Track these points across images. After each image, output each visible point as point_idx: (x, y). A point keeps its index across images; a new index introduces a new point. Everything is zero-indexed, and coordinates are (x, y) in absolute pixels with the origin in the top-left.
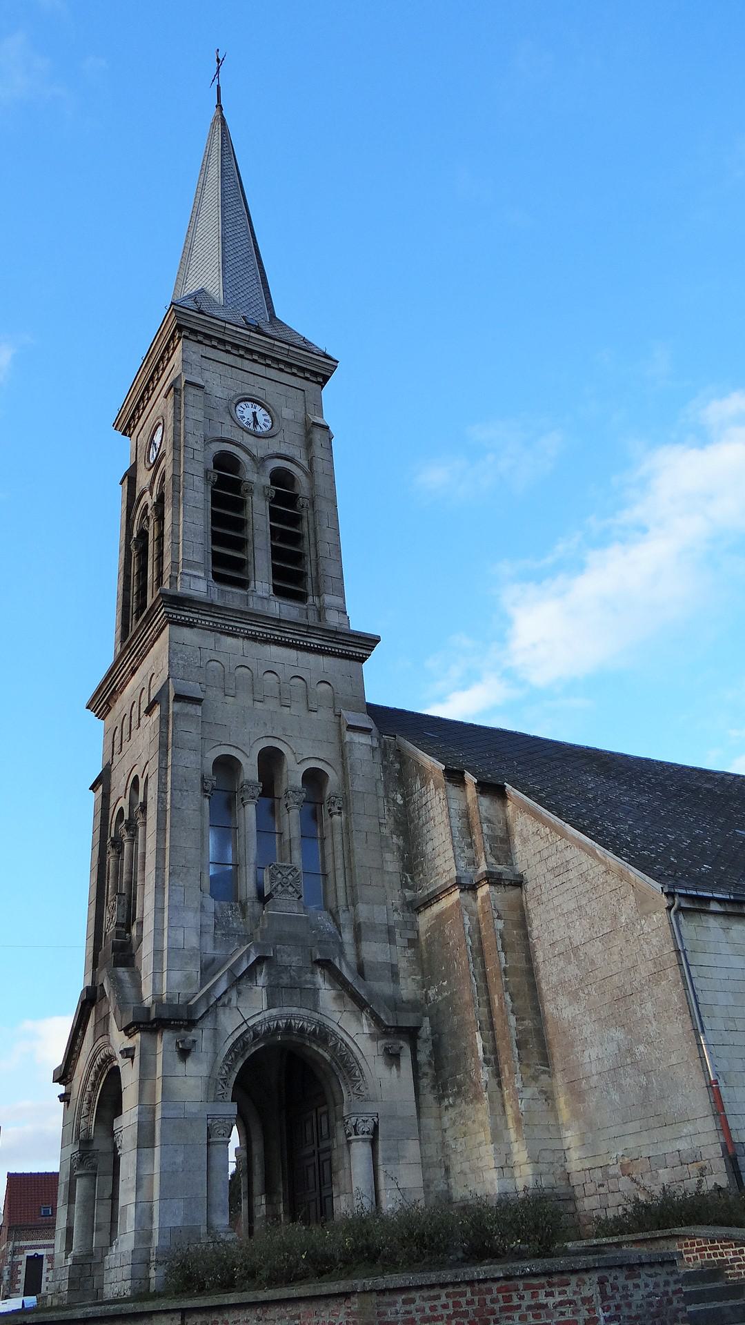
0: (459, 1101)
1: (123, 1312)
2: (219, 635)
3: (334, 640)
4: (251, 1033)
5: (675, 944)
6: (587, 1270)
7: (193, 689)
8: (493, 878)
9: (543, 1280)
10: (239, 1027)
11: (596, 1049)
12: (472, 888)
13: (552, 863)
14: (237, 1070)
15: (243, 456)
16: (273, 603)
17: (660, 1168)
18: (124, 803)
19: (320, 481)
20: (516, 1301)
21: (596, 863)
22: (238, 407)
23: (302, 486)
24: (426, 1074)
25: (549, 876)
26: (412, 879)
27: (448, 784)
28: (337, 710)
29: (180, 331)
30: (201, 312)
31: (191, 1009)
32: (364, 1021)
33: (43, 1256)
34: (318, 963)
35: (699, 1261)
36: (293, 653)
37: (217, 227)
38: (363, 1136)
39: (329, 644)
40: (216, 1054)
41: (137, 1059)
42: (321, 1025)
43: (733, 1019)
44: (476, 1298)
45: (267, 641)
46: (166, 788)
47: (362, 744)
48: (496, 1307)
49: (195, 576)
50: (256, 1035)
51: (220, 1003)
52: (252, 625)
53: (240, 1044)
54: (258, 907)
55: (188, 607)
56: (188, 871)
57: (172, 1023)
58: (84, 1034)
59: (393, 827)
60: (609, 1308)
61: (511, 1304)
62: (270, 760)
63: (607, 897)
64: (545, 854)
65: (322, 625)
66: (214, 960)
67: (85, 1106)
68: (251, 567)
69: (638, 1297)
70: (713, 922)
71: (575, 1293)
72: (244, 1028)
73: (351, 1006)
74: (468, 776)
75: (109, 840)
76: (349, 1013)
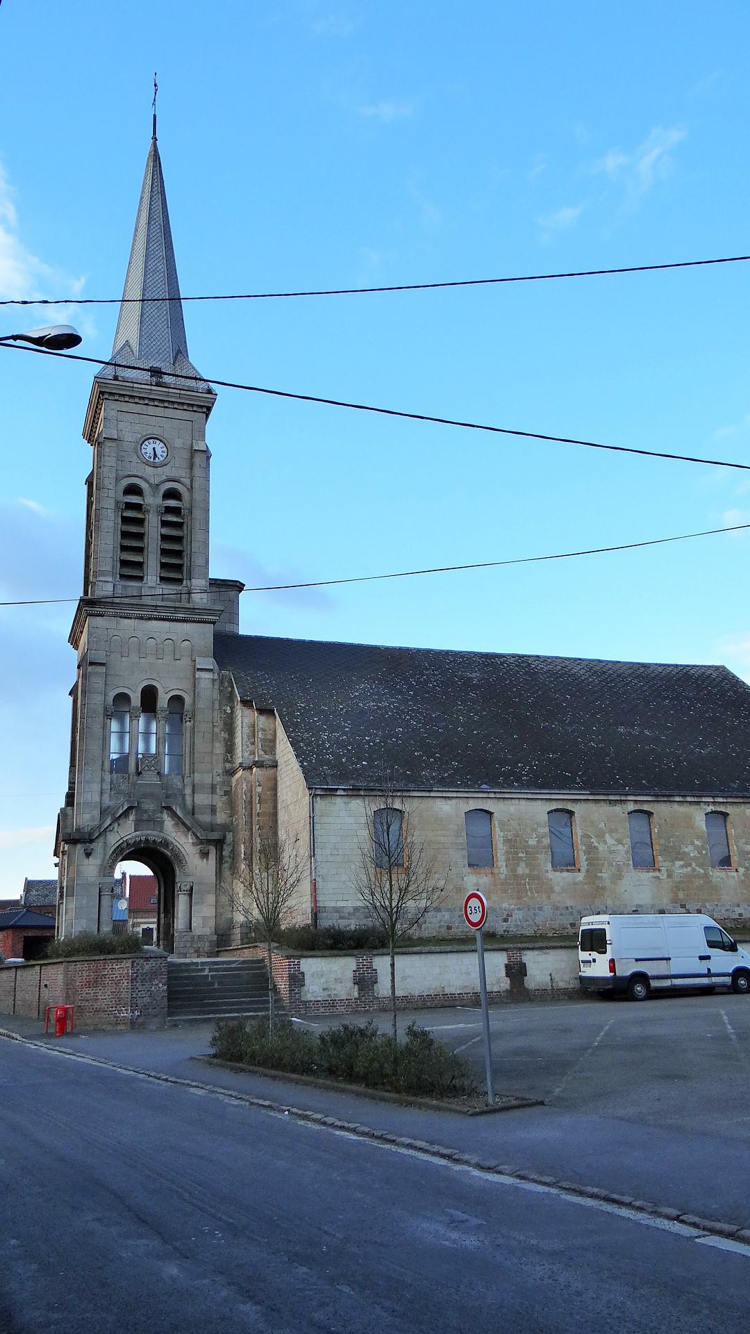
2: (119, 619)
5: (310, 814)
6: (129, 959)
7: (100, 656)
9: (116, 961)
12: (250, 768)
15: (144, 485)
19: (197, 496)
20: (107, 967)
22: (143, 446)
24: (226, 862)
26: (231, 757)
28: (193, 658)
29: (103, 395)
31: (90, 834)
32: (190, 836)
33: (153, 929)
34: (163, 807)
36: (167, 624)
38: (185, 892)
39: (191, 616)
40: (105, 854)
42: (166, 840)
43: (337, 850)
45: (150, 619)
47: (206, 679)
49: (105, 582)
50: (128, 845)
54: (135, 778)
62: (149, 696)
65: (190, 606)
68: (145, 566)
69: (147, 967)
70: (338, 800)
72: (121, 841)
73: (183, 829)
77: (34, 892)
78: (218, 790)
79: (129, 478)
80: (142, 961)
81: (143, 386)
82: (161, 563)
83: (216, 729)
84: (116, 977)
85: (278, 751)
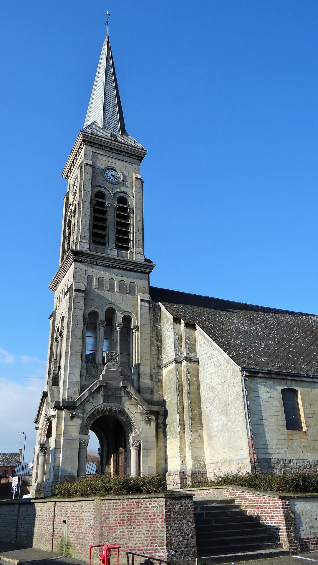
0: (171, 437)
1: (22, 502)
2: (93, 265)
3: (137, 266)
4: (97, 411)
5: (243, 389)
8: (188, 359)
9: (149, 500)
10: (92, 409)
13: (208, 355)
14: (91, 424)
16: (115, 251)
18: (59, 325)
20: (140, 506)
21: (221, 357)
22: (106, 172)
23: (132, 203)
25: (207, 359)
27: (175, 323)
29: (84, 142)
30: (92, 134)
31: (75, 403)
35: (229, 497)
37: (102, 93)
39: (136, 268)
41: (56, 419)
44: (129, 504)
45: (111, 267)
46: (70, 323)
47: (145, 306)
48: (134, 507)
49: (85, 242)
50: (98, 412)
52: (105, 261)
53: (92, 415)
55: (81, 255)
57: (68, 407)
58: (43, 407)
59: (155, 337)
60: (167, 509)
61: (139, 506)
64: (207, 351)
66: (85, 385)
67: (43, 432)
68: (107, 237)
69: (177, 507)
70: (259, 380)
71: (158, 504)
72: (94, 409)
74: (182, 320)
75: (54, 338)
76: (133, 405)
78: (154, 378)
79: (98, 188)
80: (173, 501)
81: (107, 140)
82: (117, 237)
84: (150, 516)
85: (198, 351)
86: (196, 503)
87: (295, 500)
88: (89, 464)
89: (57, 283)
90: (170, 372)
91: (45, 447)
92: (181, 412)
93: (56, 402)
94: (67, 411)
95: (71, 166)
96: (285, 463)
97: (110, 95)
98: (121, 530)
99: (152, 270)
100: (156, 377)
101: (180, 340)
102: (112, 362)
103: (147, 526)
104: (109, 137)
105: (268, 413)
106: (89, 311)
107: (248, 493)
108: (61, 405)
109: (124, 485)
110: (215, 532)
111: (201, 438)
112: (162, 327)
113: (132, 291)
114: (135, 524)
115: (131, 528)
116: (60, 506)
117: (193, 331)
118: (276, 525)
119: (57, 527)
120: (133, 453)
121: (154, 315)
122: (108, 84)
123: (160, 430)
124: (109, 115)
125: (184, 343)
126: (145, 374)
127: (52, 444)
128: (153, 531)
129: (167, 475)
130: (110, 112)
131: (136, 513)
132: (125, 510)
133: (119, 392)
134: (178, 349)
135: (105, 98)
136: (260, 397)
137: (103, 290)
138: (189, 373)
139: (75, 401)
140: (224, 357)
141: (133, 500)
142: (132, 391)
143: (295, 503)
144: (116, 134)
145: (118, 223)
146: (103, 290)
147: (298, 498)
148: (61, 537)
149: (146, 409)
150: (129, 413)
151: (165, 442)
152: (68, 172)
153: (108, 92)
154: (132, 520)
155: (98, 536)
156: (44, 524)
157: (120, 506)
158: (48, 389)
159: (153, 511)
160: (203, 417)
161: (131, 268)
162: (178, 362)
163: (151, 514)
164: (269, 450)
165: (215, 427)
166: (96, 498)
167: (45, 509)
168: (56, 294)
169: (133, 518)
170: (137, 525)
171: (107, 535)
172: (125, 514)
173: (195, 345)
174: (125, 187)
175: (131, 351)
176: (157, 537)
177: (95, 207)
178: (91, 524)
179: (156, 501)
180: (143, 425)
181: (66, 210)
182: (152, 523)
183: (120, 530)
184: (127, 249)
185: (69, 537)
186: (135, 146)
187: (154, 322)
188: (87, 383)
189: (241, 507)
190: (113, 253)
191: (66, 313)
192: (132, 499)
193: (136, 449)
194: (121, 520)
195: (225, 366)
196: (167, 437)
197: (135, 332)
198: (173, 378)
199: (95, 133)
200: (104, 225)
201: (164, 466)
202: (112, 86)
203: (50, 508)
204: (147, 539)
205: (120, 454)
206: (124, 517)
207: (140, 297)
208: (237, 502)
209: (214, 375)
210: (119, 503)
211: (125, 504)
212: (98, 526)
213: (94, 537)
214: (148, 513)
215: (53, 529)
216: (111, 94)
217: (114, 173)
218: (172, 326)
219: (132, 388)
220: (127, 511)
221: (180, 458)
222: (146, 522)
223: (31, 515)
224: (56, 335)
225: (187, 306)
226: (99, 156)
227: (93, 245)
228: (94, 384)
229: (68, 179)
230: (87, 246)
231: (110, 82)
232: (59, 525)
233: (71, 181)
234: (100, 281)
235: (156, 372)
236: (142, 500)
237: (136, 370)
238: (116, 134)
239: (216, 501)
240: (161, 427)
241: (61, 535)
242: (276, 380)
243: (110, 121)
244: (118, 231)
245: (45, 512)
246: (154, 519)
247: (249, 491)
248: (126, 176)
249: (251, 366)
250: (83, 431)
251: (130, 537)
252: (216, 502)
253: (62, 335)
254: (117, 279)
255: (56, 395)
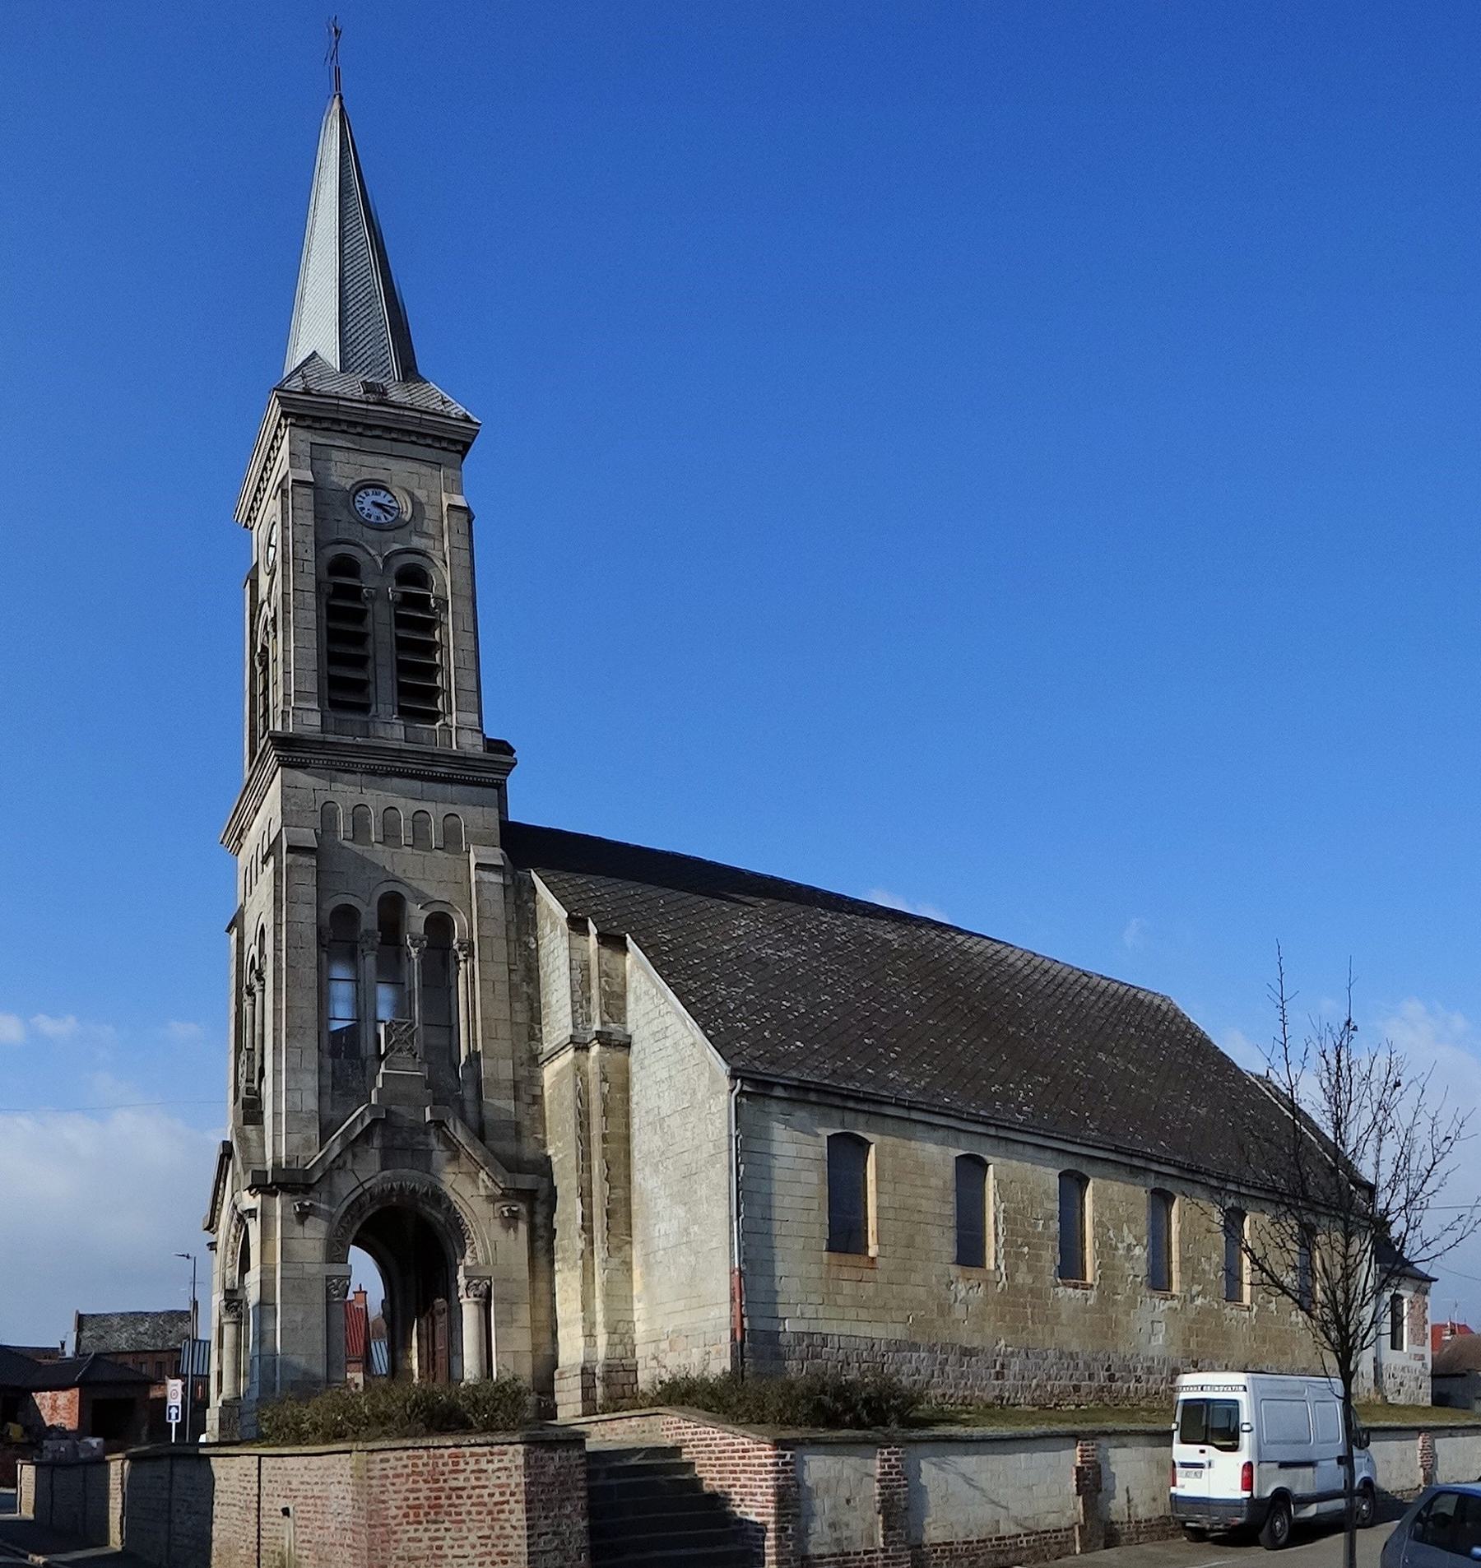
2: (334, 773)
4: (368, 1197)
5: (730, 1130)
8: (604, 1038)
9: (486, 1449)
11: (664, 1224)
17: (694, 1347)
18: (255, 950)
20: (462, 1466)
22: (358, 498)
23: (443, 579)
30: (307, 392)
31: (307, 1173)
35: (674, 1438)
45: (388, 774)
47: (491, 883)
48: (446, 1469)
49: (308, 709)
51: (335, 1165)
53: (357, 1206)
56: (305, 1032)
59: (523, 973)
63: (691, 1070)
64: (651, 1015)
66: (332, 1120)
67: (229, 1256)
68: (371, 688)
70: (774, 1107)
71: (510, 1461)
72: (360, 1190)
74: (591, 924)
76: (464, 1176)
77: (87, 1334)
81: (354, 405)
82: (400, 685)
83: (513, 977)
84: (491, 1495)
86: (596, 1455)
87: (805, 1449)
88: (377, 1344)
89: (242, 830)
90: (560, 1073)
91: (236, 1301)
92: (585, 1194)
93: (254, 1172)
94: (287, 1197)
95: (258, 489)
96: (814, 1342)
97: (355, 269)
98: (412, 1534)
99: (508, 775)
100: (527, 1089)
101: (586, 983)
102: (400, 1050)
103: (483, 1524)
104: (360, 393)
105: (787, 1201)
106: (330, 906)
107: (711, 1429)
108: (270, 1181)
109: (419, 1408)
110: (675, 1533)
111: (627, 1265)
112: (540, 943)
113: (452, 840)
114: (450, 1518)
115: (437, 1530)
116: (273, 1468)
117: (618, 957)
118: (759, 1519)
119: (268, 1527)
120: (469, 1313)
121: (518, 907)
122: (349, 238)
123: (540, 1244)
124: (356, 328)
125: (595, 992)
126: (497, 1082)
127: (253, 1295)
128: (498, 1538)
129: (556, 1376)
130: (358, 318)
131: (450, 1489)
132: (420, 1479)
133: (421, 1138)
134: (581, 1007)
135: (342, 279)
136: (774, 1156)
137: (368, 842)
138: (605, 1080)
139: (308, 1167)
140: (693, 1036)
141: (442, 1451)
142: (460, 1135)
143: (806, 1458)
144: (382, 381)
145: (402, 644)
146: (368, 842)
147: (815, 1442)
148: (279, 1554)
149: (502, 1186)
150: (452, 1199)
151: (552, 1281)
152: (252, 508)
153: (348, 262)
154: (441, 1506)
155: (365, 1553)
156: (234, 1515)
157: (406, 1466)
158: (235, 1136)
159: (498, 1482)
160: (634, 1207)
161: (445, 773)
162: (582, 1047)
163: (492, 1491)
164: (780, 1307)
165: (659, 1237)
166: (355, 1445)
167: (234, 1474)
168: (243, 859)
169: (443, 1501)
170: (453, 1522)
171: (383, 1550)
172: (420, 1490)
173: (622, 997)
174: (422, 537)
175: (454, 1015)
176: (511, 1554)
177: (332, 603)
178: (347, 1519)
179: (506, 1454)
180: (497, 1230)
181: (252, 616)
182: (495, 1516)
183: (409, 1535)
184: (433, 717)
185: (300, 1557)
186: (445, 414)
187: (518, 929)
188: (337, 1114)
189: (697, 1469)
190: (394, 732)
191: (268, 920)
192: (439, 1447)
193: (476, 1303)
194: (409, 1507)
195: (694, 1062)
196: (557, 1266)
197: (466, 961)
198: (569, 1094)
199: (315, 387)
200: (360, 652)
201: (549, 1352)
202: (361, 241)
203: (247, 1473)
204: (484, 1562)
205: (437, 1317)
206: (418, 1499)
207: (476, 856)
208: (687, 1453)
209: (665, 1086)
210: (392, 1460)
211: (420, 1462)
212: (363, 1525)
213: (354, 1556)
214: (485, 1487)
215: (259, 1531)
216: (359, 266)
217: (382, 498)
218: (566, 938)
219: (458, 1125)
220: (426, 1481)
221: (583, 1327)
222: (479, 1513)
223: (202, 1489)
224: (249, 978)
225: (604, 881)
226: (336, 455)
227: (333, 714)
228: (358, 1117)
229: (252, 528)
230: (316, 719)
231: (355, 229)
232: (271, 1520)
233: (259, 533)
234: (359, 815)
235: (526, 1074)
236: (467, 1451)
237: (469, 1071)
238: (382, 381)
239: (642, 1450)
240: (542, 1237)
241: (280, 1550)
242: (816, 1109)
243: (362, 345)
244: (403, 668)
245: (238, 1484)
246: (503, 1503)
247: (714, 1424)
248: (421, 504)
249: (757, 1064)
250: (335, 1253)
251: (435, 1556)
252: (641, 1455)
253: (264, 980)
254: (406, 808)
255: (255, 1151)
